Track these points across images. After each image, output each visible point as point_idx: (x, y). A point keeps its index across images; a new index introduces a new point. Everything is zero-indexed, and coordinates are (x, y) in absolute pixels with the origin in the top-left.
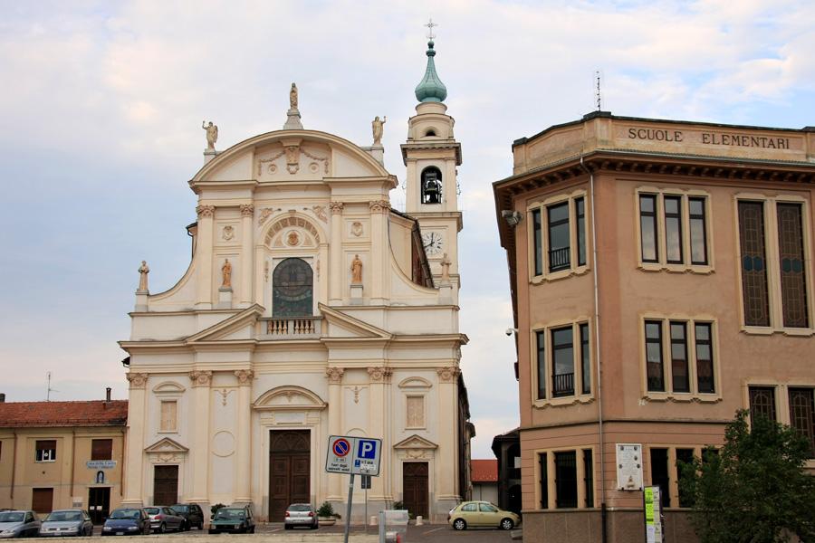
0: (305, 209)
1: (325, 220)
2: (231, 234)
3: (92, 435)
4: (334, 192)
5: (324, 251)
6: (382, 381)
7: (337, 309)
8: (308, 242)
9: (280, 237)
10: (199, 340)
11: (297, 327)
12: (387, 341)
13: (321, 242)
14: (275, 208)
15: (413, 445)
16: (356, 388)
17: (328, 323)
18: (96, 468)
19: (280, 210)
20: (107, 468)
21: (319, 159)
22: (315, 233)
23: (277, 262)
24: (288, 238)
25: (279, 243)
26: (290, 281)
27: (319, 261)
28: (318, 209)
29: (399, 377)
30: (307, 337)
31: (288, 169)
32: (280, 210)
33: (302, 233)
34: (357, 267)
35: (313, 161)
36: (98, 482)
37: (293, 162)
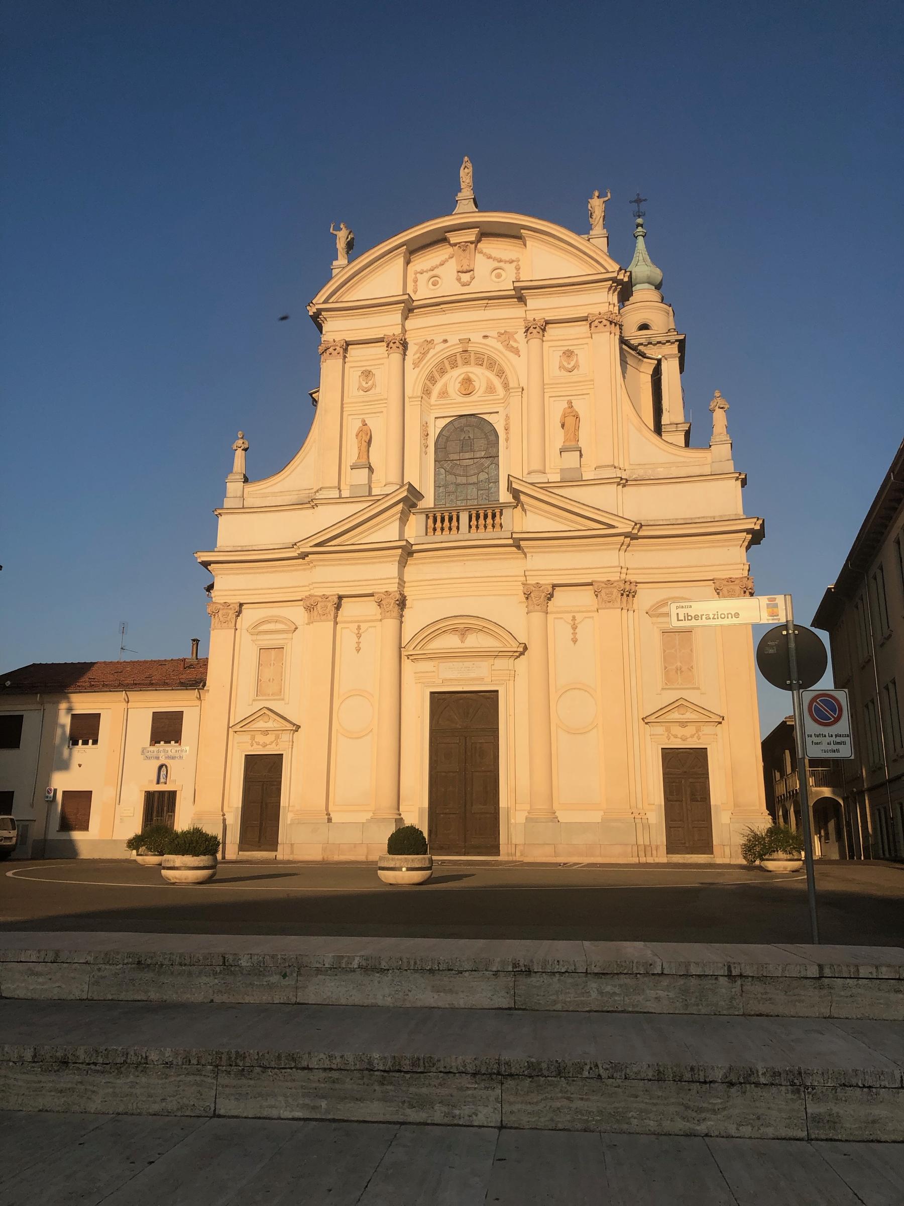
0: (485, 337)
1: (517, 352)
2: (572, 363)
3: (151, 705)
4: (532, 303)
5: (515, 400)
6: (618, 605)
7: (545, 487)
8: (491, 389)
9: (446, 385)
10: (317, 545)
11: (474, 522)
12: (626, 535)
13: (511, 385)
14: (438, 339)
15: (675, 716)
16: (574, 618)
17: (524, 510)
18: (158, 758)
19: (445, 341)
20: (173, 758)
21: (506, 262)
22: (501, 373)
23: (443, 423)
24: (458, 386)
25: (444, 394)
26: (462, 451)
27: (507, 417)
28: (506, 337)
29: (646, 598)
30: (489, 536)
31: (459, 280)
32: (445, 341)
33: (481, 376)
34: (570, 421)
35: (497, 264)
36: (158, 782)
37: (465, 268)
